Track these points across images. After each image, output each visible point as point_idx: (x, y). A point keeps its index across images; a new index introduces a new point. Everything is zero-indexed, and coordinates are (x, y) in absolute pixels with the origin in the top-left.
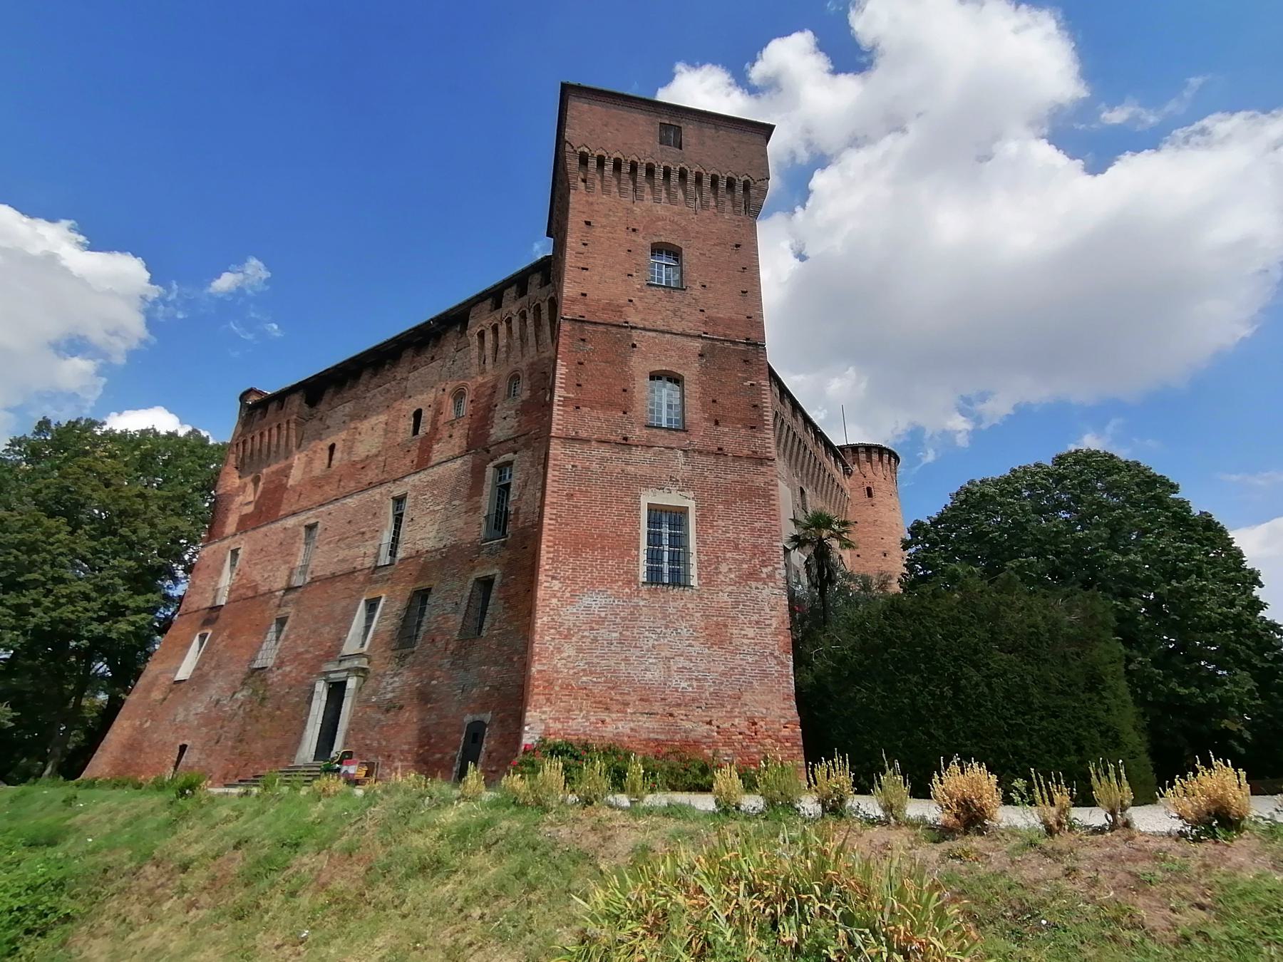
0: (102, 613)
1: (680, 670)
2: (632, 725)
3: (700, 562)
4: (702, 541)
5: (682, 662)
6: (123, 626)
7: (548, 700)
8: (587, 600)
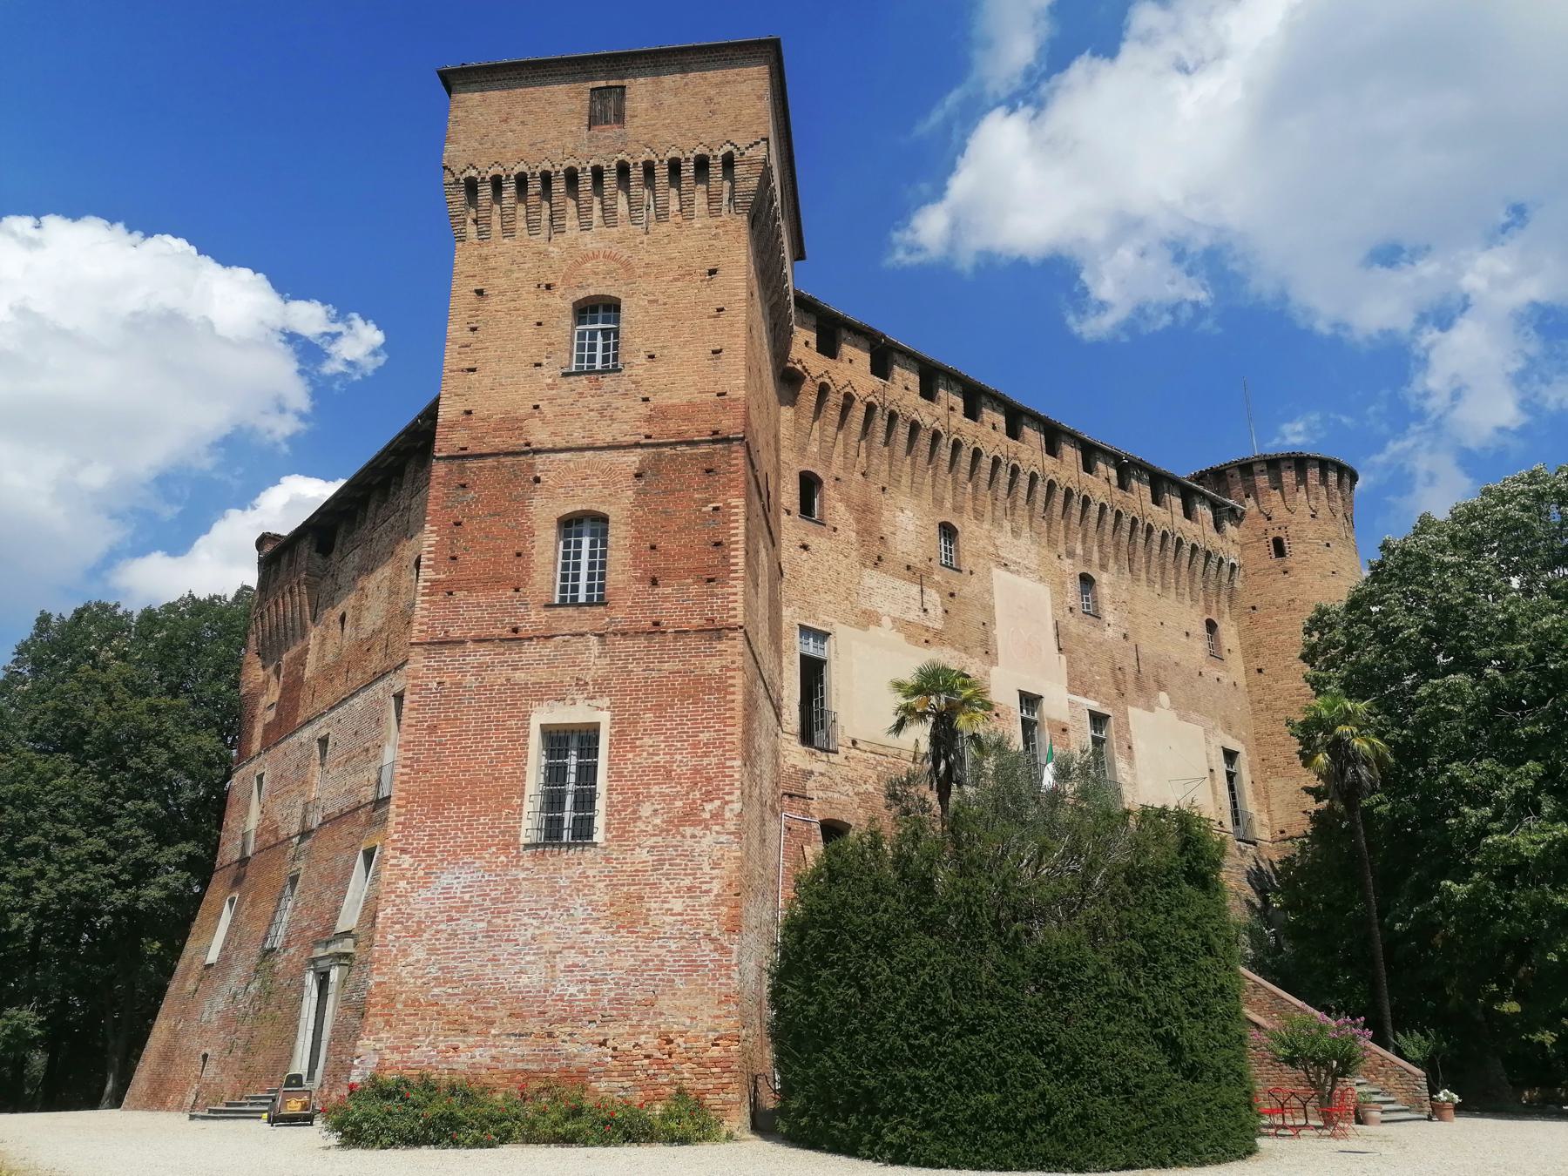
0: (126, 877)
1: (570, 969)
2: (494, 1051)
3: (610, 805)
4: (616, 774)
5: (572, 957)
6: (153, 893)
7: (387, 1023)
8: (446, 879)
